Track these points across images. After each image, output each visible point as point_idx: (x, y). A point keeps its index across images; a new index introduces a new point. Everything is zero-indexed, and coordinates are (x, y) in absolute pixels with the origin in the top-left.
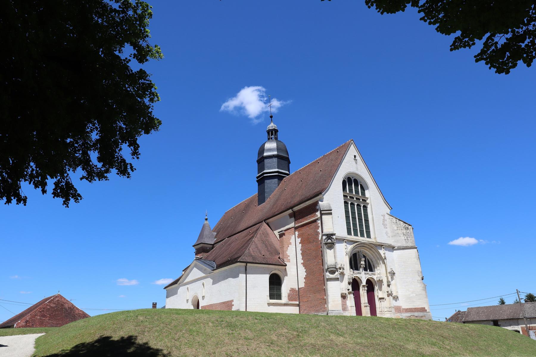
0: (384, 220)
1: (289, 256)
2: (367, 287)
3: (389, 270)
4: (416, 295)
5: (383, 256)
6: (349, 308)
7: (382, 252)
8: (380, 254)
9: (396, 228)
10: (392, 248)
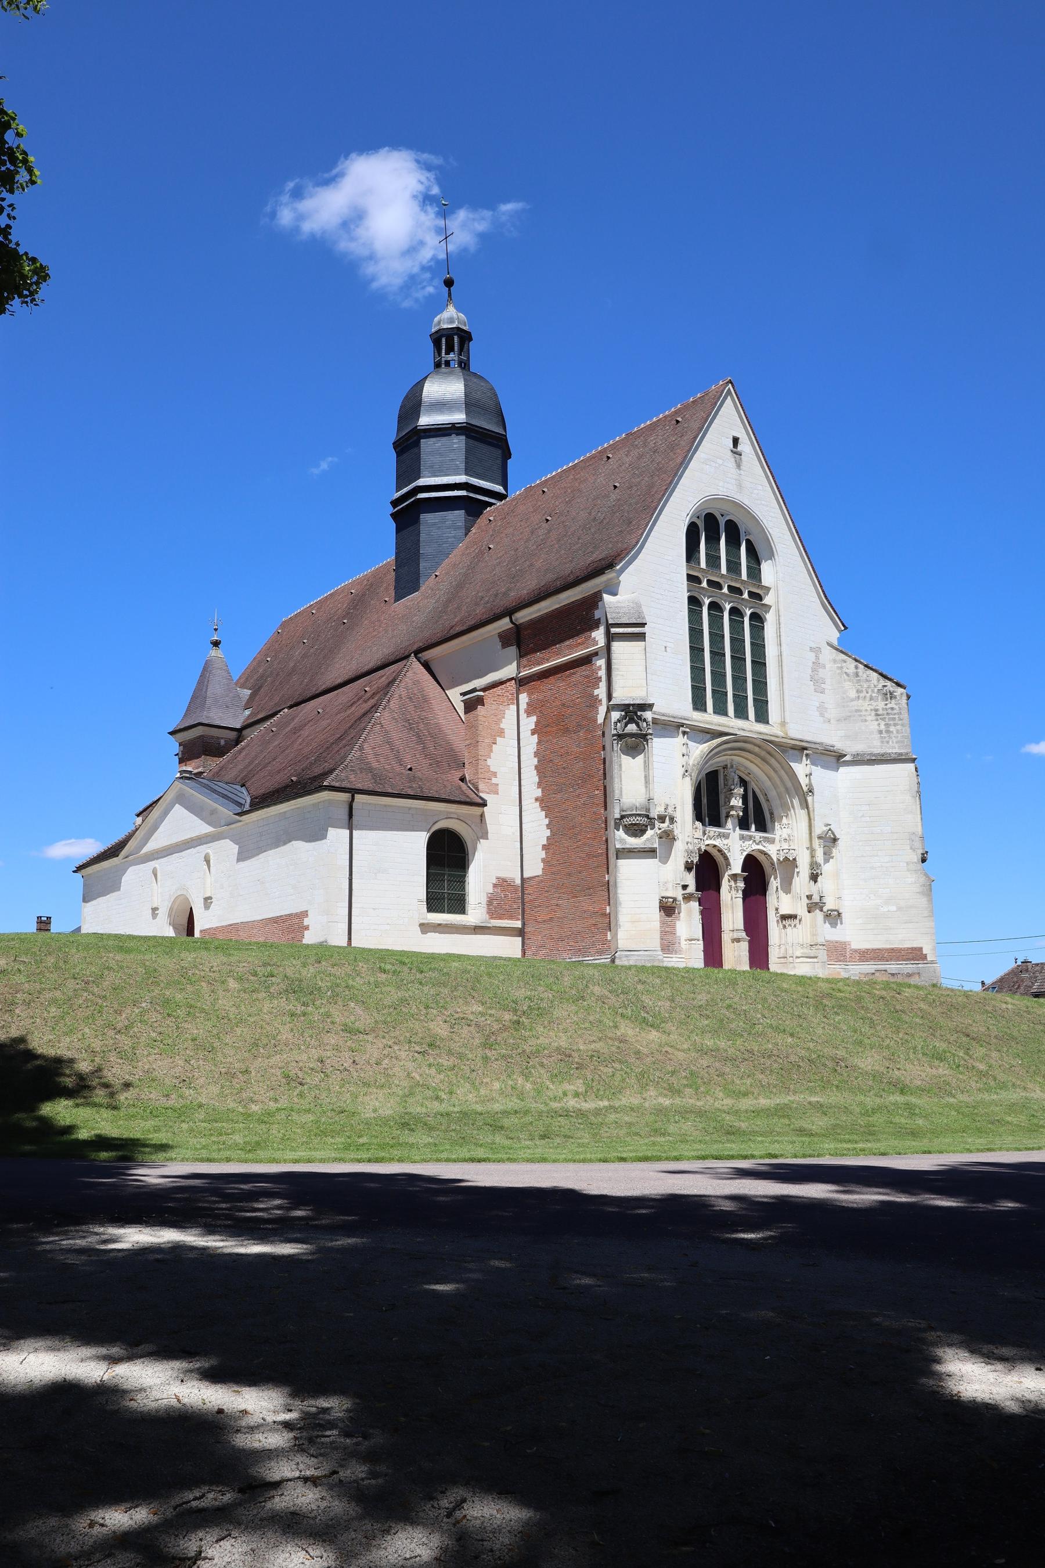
0: (817, 665)
1: (495, 774)
2: (745, 880)
3: (819, 829)
4: (899, 909)
5: (804, 781)
6: (683, 943)
7: (801, 768)
8: (793, 776)
9: (853, 694)
10: (835, 758)
